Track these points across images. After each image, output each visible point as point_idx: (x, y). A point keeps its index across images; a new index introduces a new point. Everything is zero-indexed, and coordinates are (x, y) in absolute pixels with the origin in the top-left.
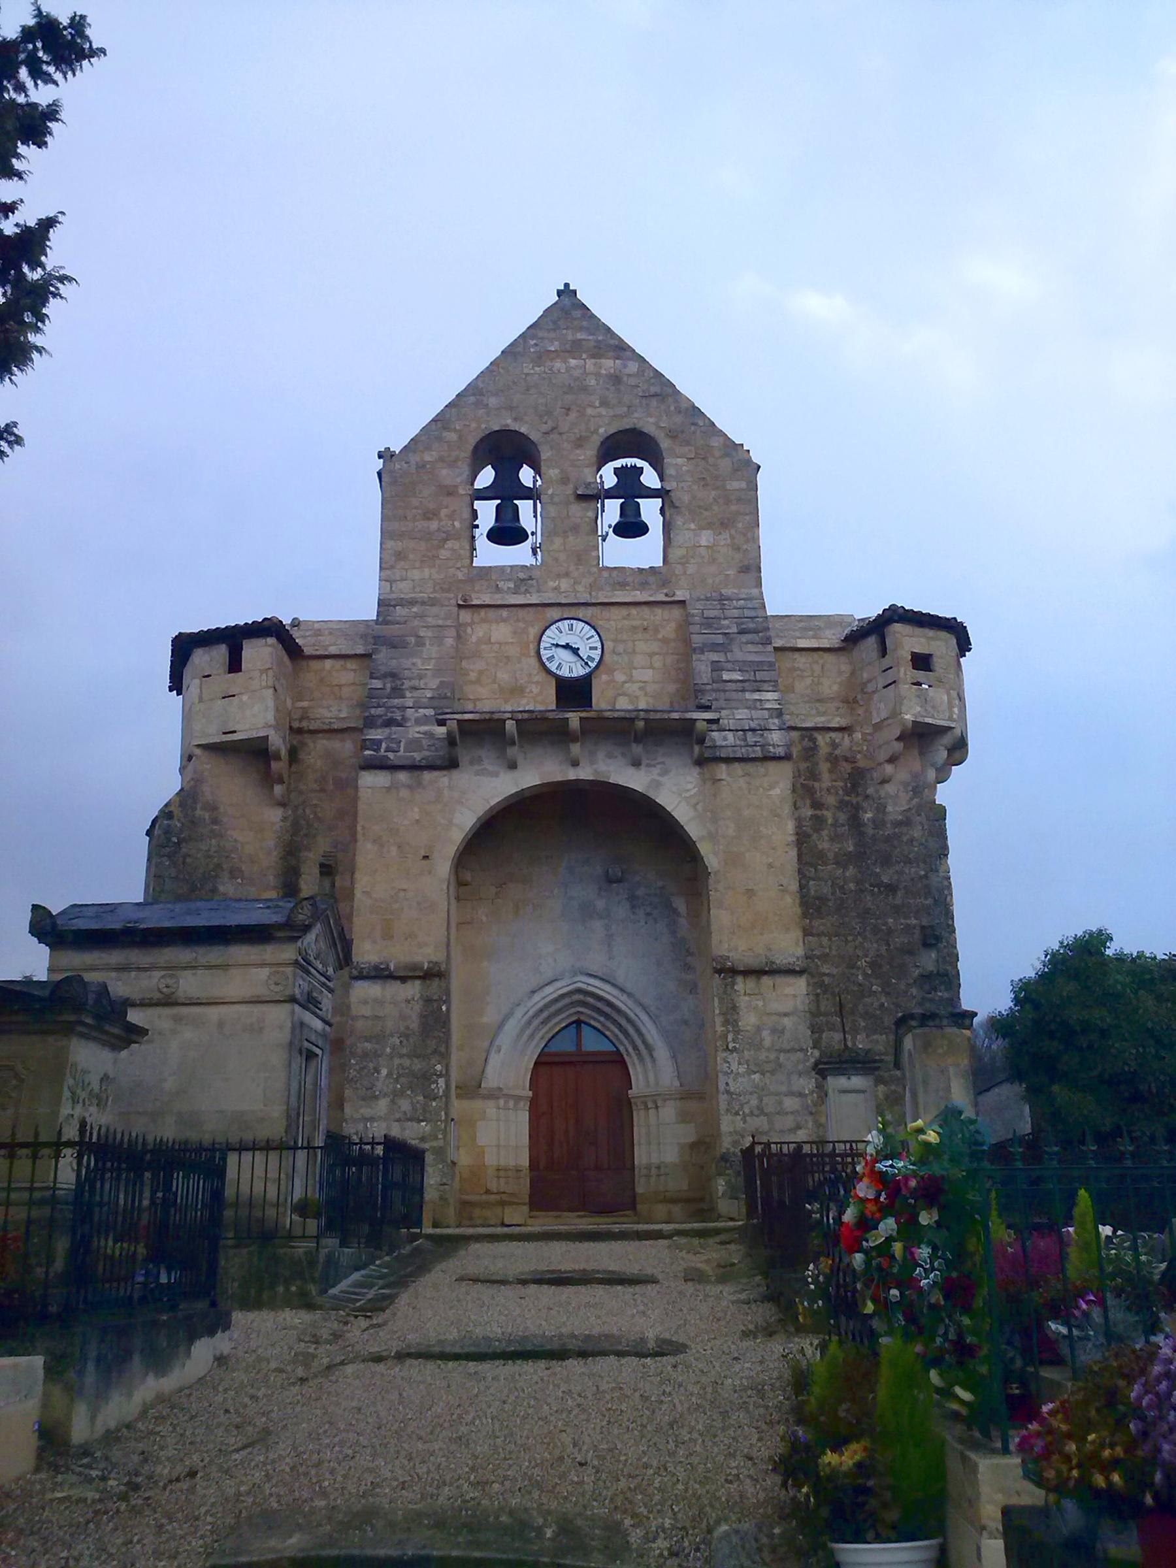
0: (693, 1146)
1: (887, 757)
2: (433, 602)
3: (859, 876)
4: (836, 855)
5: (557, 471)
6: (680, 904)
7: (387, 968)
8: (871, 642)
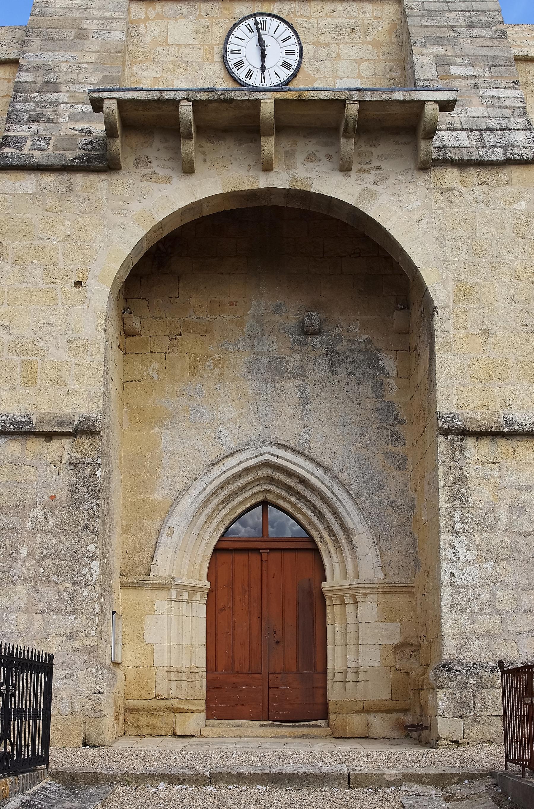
0: (397, 648)
6: (388, 362)
7: (29, 423)
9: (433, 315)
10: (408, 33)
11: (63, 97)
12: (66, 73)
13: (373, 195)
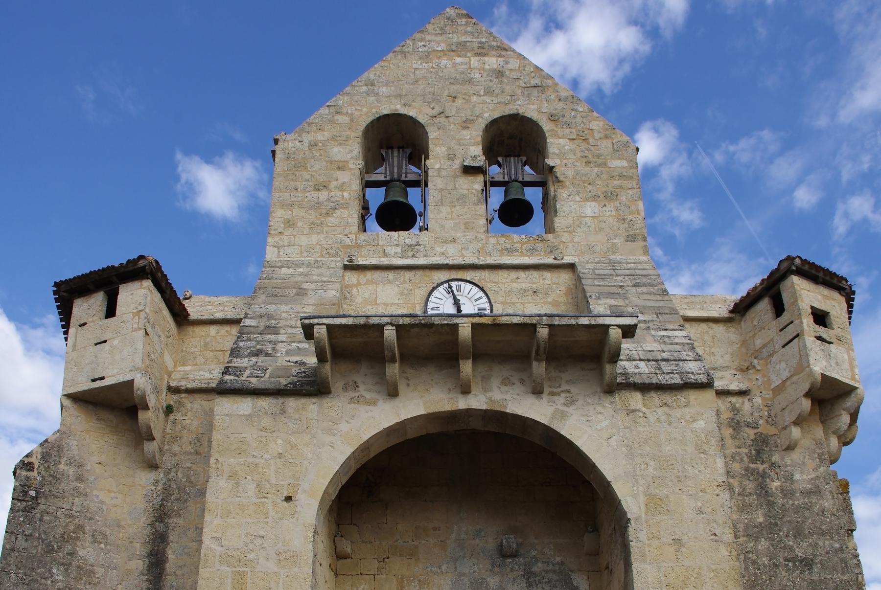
1: (793, 419)
2: (318, 265)
3: (772, 548)
4: (747, 527)
5: (444, 149)
8: (765, 306)
9: (626, 527)
10: (584, 290)
11: (282, 337)
12: (286, 320)
13: (564, 415)
